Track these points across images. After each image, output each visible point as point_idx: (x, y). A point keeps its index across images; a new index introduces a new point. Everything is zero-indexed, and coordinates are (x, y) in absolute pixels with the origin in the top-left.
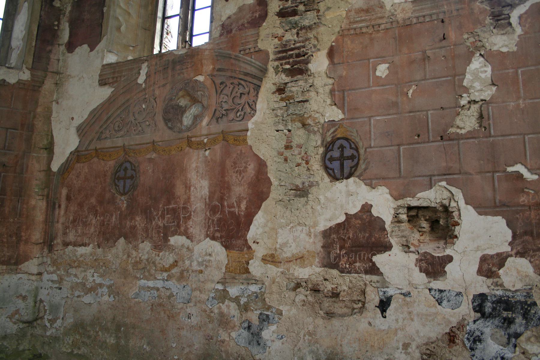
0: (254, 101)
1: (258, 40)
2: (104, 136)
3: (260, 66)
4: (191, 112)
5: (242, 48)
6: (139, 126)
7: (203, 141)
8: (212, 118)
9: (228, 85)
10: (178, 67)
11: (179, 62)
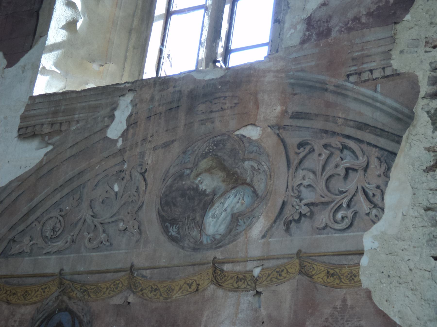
0: (378, 187)
1: (391, 52)
2: (16, 248)
3: (396, 109)
4: (226, 205)
5: (353, 68)
6: (101, 231)
7: (251, 271)
8: (275, 222)
9: (316, 148)
10: (202, 107)
11: (205, 95)
